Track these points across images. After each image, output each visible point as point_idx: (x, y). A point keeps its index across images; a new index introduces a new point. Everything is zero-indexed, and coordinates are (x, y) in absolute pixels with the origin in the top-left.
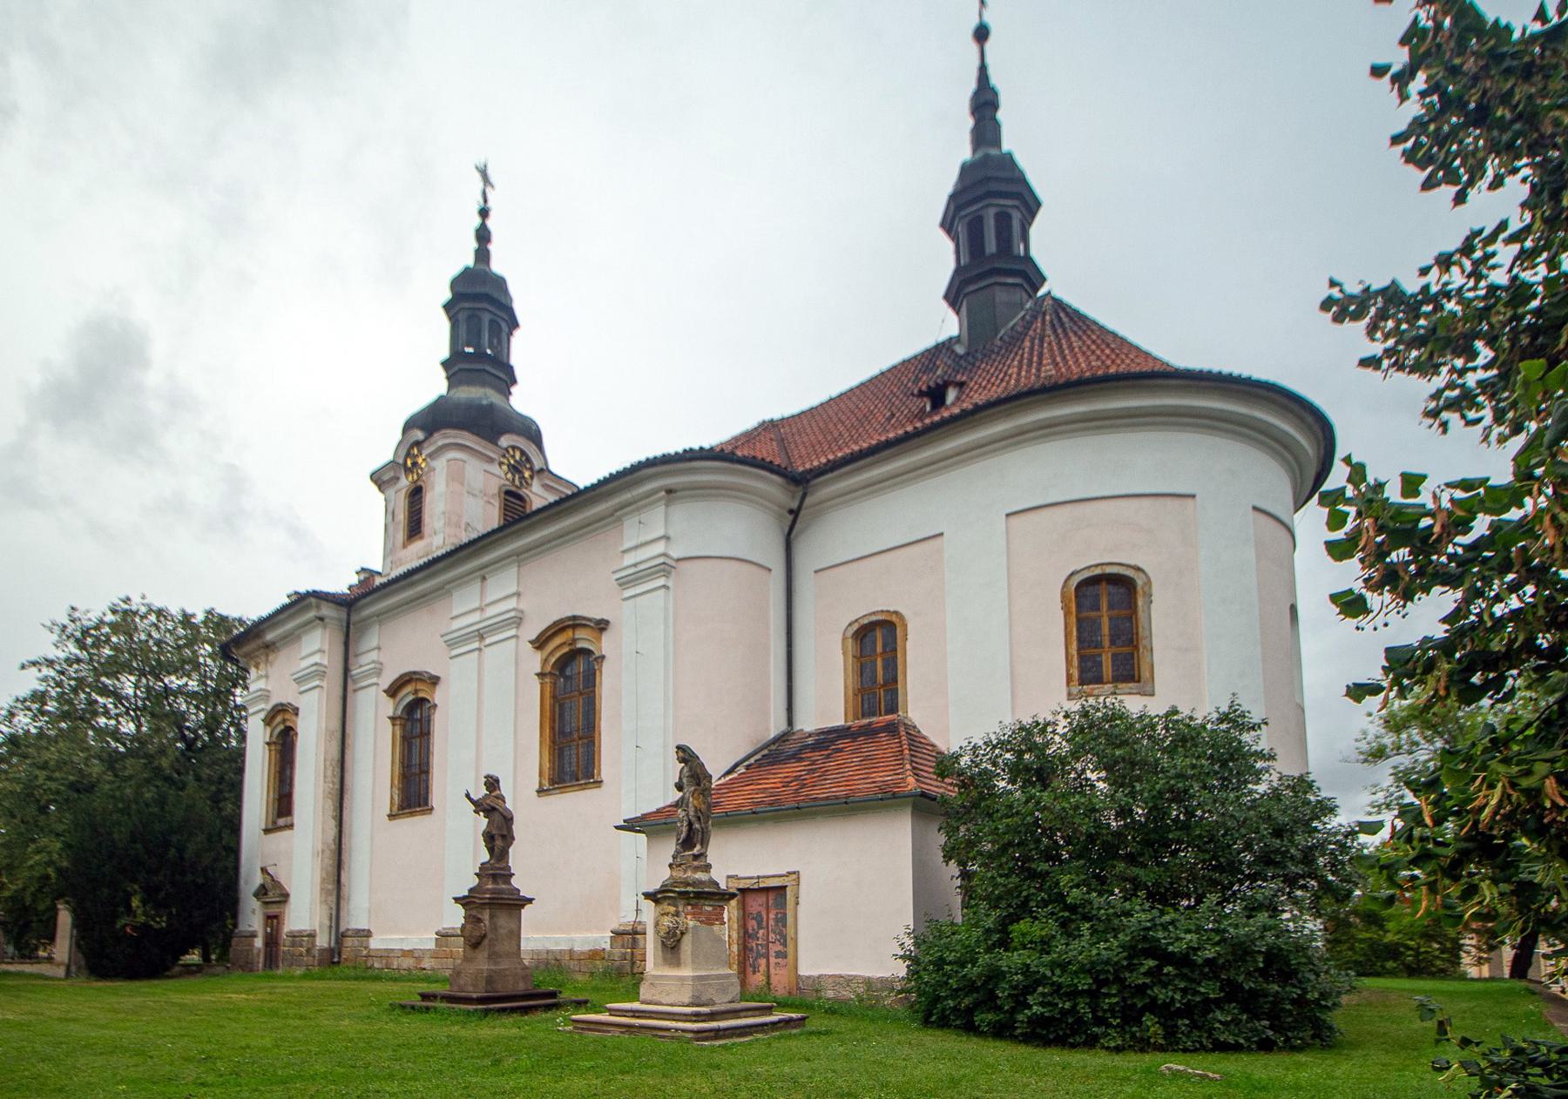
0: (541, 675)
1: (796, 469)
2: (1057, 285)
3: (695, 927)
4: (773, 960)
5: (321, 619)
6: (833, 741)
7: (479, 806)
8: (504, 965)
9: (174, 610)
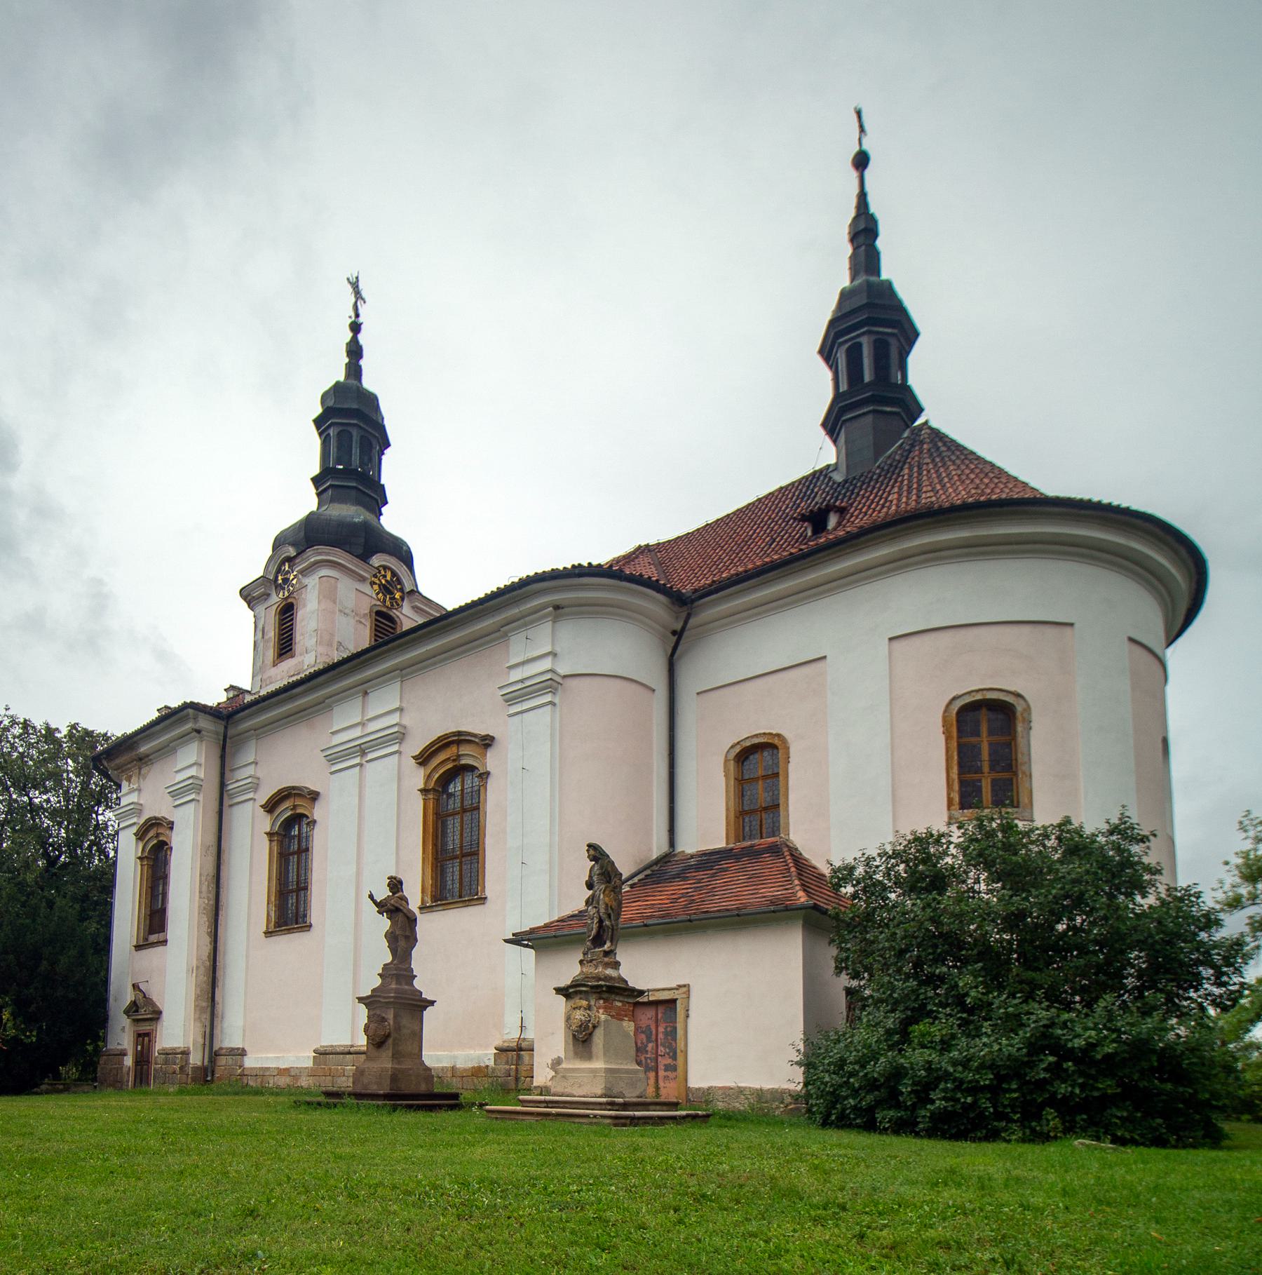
0: (424, 791)
1: (677, 594)
2: (935, 415)
3: (606, 1021)
4: (662, 1073)
5: (198, 732)
6: (717, 862)
7: (382, 907)
8: (407, 1065)
9: (38, 723)
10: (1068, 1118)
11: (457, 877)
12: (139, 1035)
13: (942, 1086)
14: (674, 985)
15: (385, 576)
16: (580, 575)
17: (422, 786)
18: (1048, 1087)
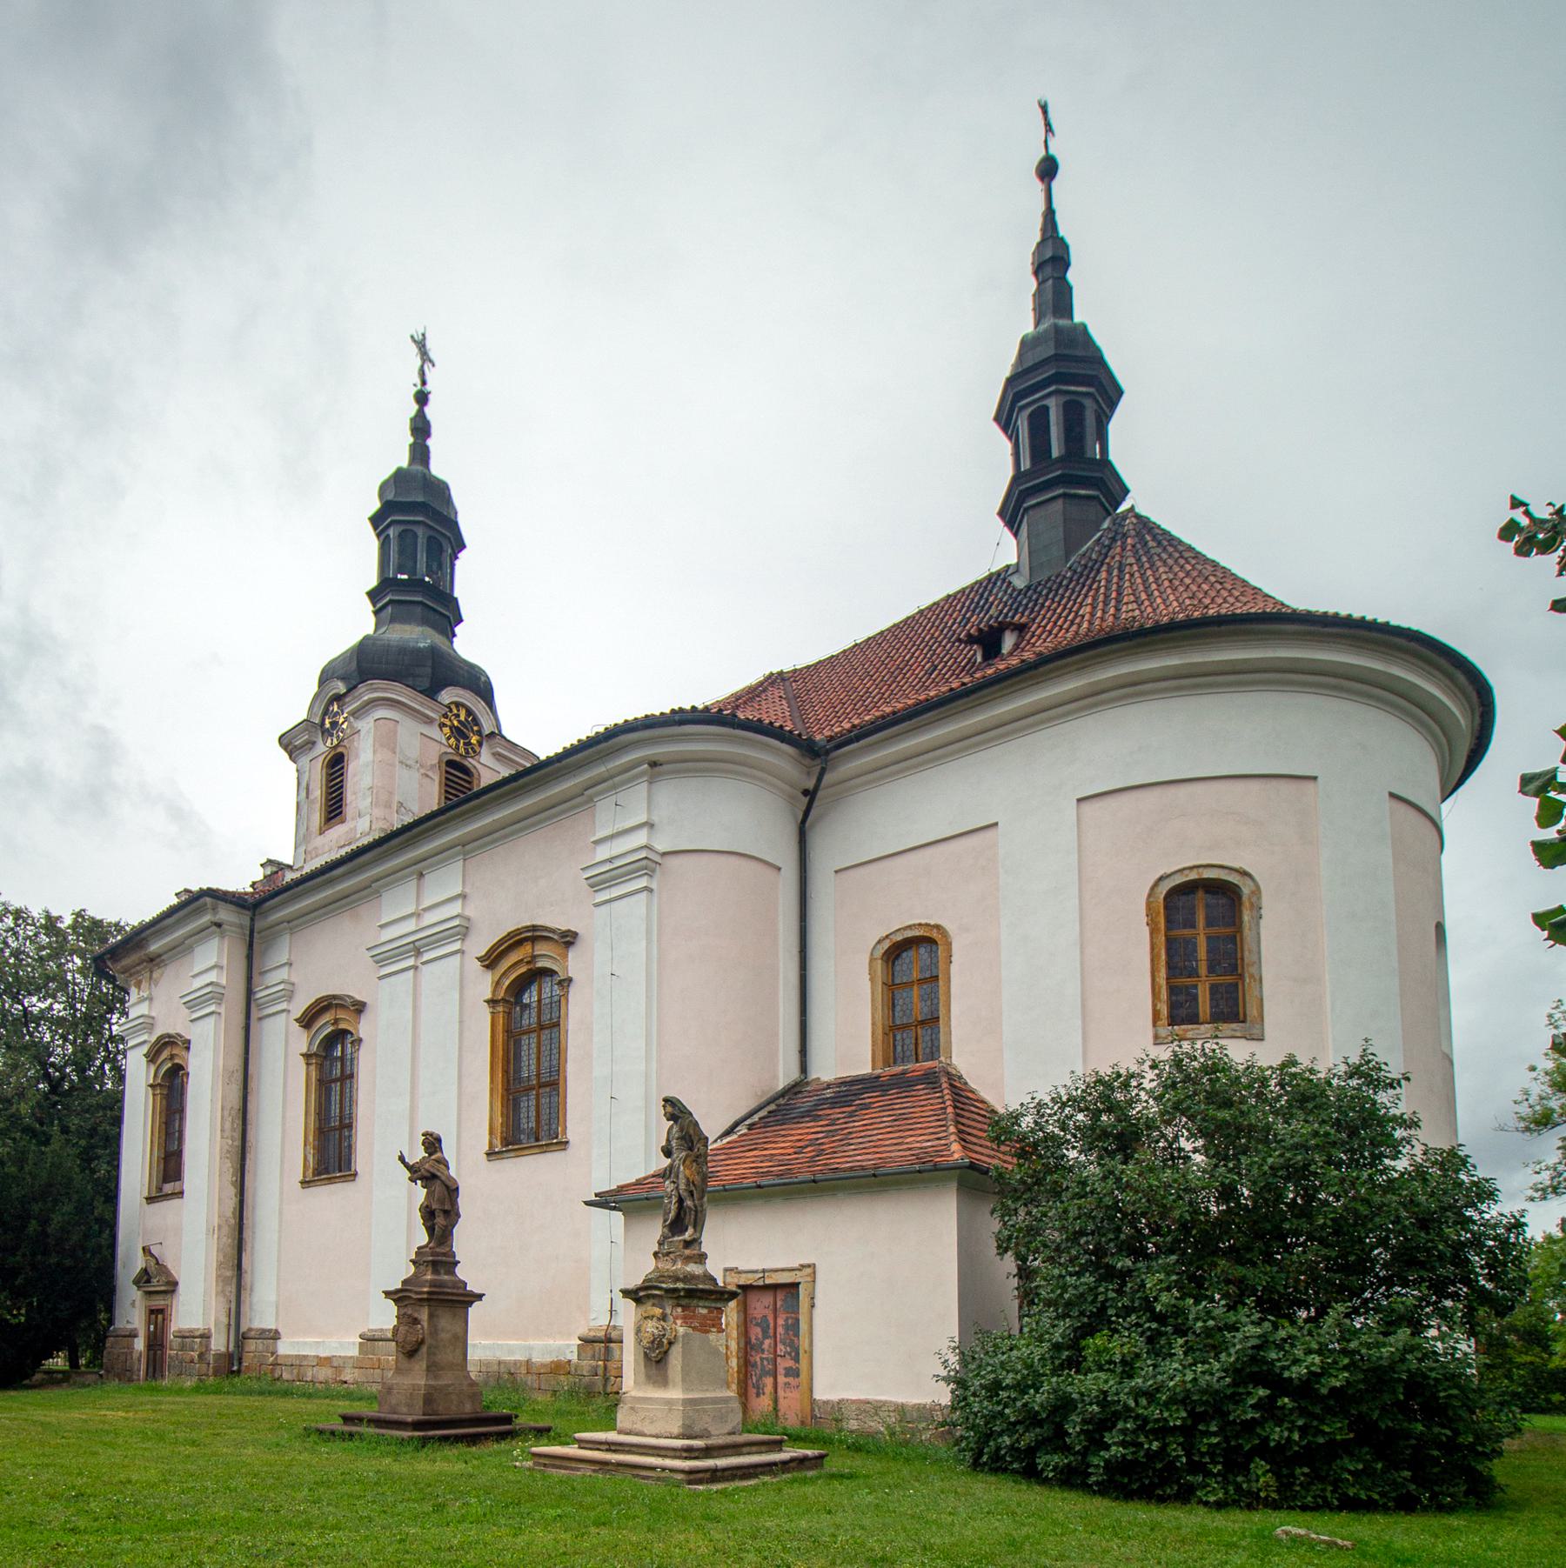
0: (492, 1002)
3: (685, 1335)
4: (781, 1379)
5: (219, 925)
8: (446, 1379)
9: (36, 912)
10: (1285, 1471)
11: (533, 1114)
12: (152, 1312)
13: (1120, 1425)
14: (796, 1265)
15: (457, 716)
16: (681, 723)
17: (489, 996)
18: (1258, 1430)
